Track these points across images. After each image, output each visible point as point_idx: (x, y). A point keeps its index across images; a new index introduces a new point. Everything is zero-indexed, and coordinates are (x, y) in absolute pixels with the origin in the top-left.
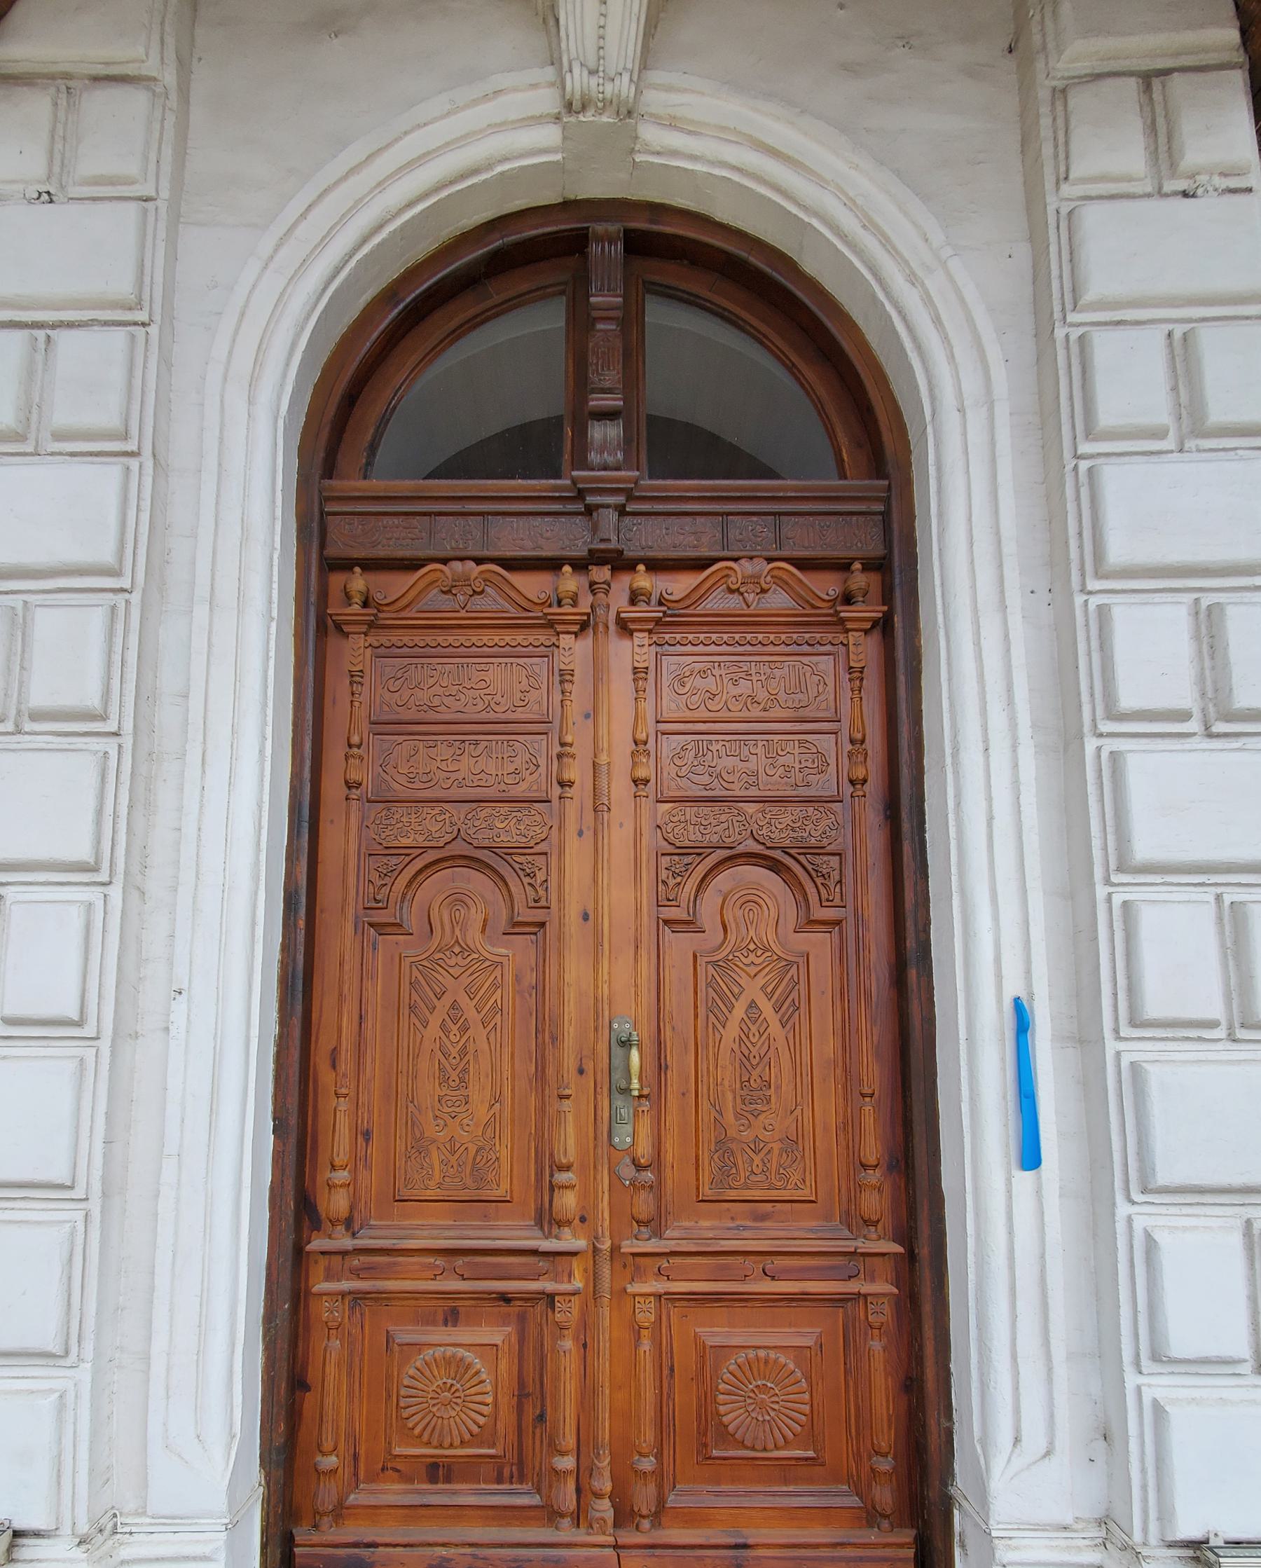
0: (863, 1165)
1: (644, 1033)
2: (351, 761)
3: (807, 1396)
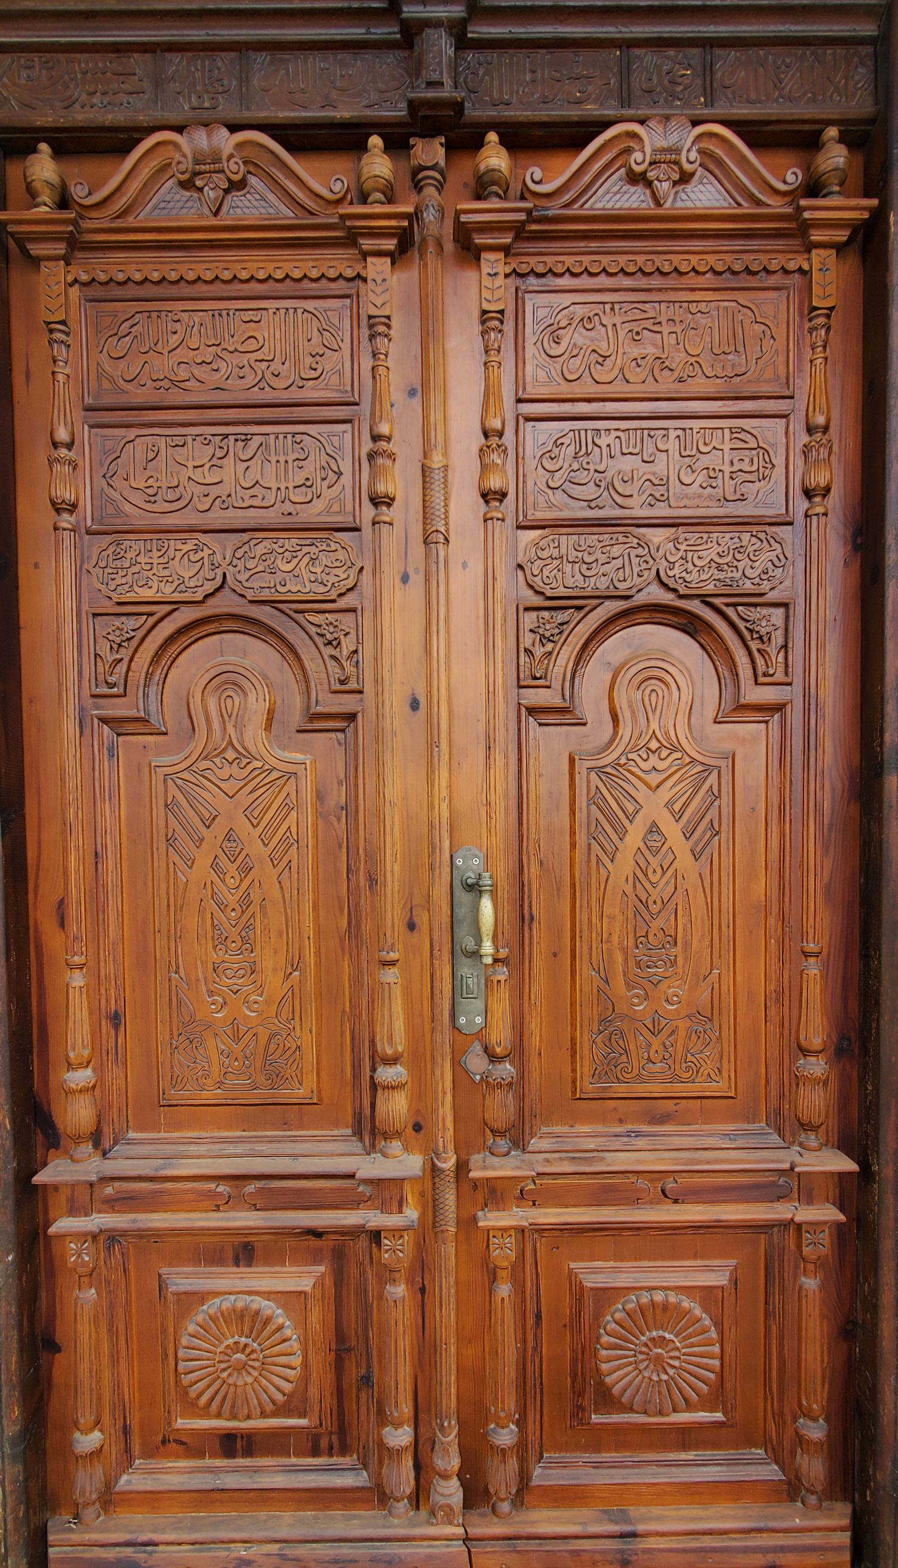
0: (800, 1048)
1: (503, 869)
2: (57, 468)
3: (716, 1349)
